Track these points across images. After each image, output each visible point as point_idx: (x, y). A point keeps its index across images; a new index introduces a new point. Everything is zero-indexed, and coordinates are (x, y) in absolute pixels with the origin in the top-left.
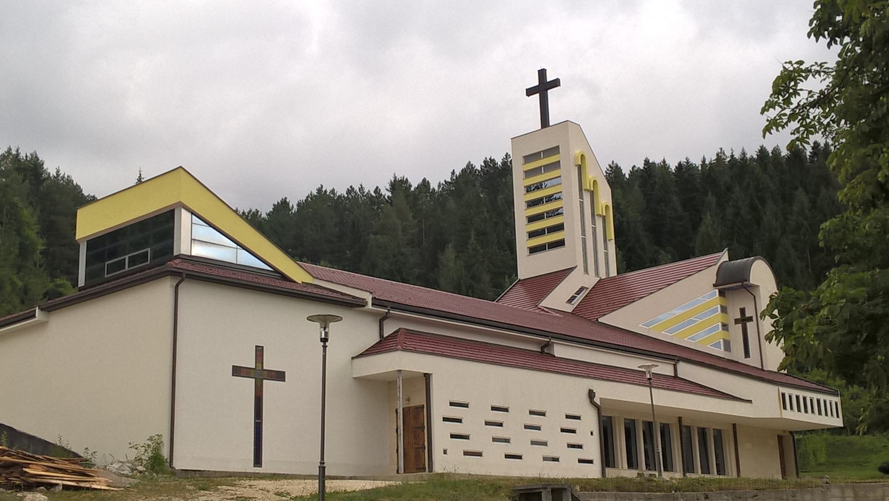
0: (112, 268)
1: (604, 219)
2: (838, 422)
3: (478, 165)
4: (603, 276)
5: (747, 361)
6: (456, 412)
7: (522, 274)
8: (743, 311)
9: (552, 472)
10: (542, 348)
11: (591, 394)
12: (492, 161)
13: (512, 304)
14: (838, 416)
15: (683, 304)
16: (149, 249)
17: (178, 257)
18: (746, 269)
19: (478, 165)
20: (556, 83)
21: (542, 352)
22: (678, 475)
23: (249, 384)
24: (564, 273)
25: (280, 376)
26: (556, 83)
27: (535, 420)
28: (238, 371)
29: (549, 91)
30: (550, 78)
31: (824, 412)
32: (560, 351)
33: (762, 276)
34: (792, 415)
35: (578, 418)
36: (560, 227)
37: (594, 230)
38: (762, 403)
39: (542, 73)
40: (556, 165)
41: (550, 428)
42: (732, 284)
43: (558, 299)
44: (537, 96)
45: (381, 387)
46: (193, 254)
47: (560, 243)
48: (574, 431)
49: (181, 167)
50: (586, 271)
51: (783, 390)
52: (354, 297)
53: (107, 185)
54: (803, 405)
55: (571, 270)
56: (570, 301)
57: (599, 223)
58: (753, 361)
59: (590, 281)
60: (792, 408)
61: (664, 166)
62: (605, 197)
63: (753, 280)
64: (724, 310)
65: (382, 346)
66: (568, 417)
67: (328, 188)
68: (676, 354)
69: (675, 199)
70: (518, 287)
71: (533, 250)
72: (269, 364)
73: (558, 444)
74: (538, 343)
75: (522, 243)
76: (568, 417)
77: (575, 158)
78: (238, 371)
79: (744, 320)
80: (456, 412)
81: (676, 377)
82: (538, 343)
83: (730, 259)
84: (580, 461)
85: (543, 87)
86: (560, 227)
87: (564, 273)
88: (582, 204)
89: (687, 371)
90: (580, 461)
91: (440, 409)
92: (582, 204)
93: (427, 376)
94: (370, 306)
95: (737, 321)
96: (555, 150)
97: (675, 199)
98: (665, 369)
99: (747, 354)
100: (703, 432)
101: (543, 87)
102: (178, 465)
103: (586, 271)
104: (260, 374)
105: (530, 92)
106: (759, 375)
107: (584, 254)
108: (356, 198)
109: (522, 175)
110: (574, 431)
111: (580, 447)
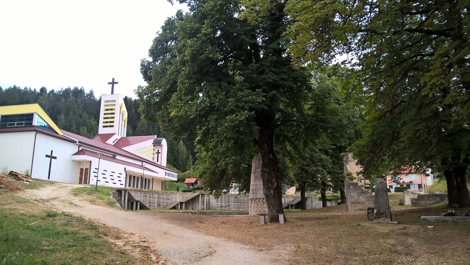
0: (9, 125)
2: (176, 180)
3: (72, 88)
7: (100, 133)
8: (158, 151)
9: (107, 185)
11: (125, 169)
13: (95, 142)
15: (144, 147)
17: (34, 126)
18: (161, 141)
19: (72, 88)
20: (117, 83)
24: (113, 134)
26: (117, 83)
27: (112, 174)
28: (47, 156)
31: (173, 176)
32: (118, 157)
33: (164, 142)
34: (167, 177)
36: (113, 122)
38: (161, 174)
39: (113, 79)
41: (116, 175)
42: (157, 144)
43: (111, 141)
47: (113, 126)
54: (169, 175)
55: (114, 134)
57: (123, 122)
58: (159, 163)
59: (119, 137)
61: (131, 99)
64: (154, 150)
65: (78, 153)
67: (17, 86)
69: (133, 110)
70: (98, 136)
71: (104, 127)
73: (116, 180)
75: (101, 124)
78: (47, 156)
79: (158, 153)
85: (113, 83)
86: (113, 122)
87: (113, 134)
91: (93, 169)
93: (91, 162)
94: (77, 143)
97: (133, 110)
98: (140, 163)
99: (158, 161)
100: (134, 177)
101: (113, 83)
102: (32, 177)
104: (51, 157)
105: (109, 83)
106: (160, 167)
107: (119, 129)
108: (27, 91)
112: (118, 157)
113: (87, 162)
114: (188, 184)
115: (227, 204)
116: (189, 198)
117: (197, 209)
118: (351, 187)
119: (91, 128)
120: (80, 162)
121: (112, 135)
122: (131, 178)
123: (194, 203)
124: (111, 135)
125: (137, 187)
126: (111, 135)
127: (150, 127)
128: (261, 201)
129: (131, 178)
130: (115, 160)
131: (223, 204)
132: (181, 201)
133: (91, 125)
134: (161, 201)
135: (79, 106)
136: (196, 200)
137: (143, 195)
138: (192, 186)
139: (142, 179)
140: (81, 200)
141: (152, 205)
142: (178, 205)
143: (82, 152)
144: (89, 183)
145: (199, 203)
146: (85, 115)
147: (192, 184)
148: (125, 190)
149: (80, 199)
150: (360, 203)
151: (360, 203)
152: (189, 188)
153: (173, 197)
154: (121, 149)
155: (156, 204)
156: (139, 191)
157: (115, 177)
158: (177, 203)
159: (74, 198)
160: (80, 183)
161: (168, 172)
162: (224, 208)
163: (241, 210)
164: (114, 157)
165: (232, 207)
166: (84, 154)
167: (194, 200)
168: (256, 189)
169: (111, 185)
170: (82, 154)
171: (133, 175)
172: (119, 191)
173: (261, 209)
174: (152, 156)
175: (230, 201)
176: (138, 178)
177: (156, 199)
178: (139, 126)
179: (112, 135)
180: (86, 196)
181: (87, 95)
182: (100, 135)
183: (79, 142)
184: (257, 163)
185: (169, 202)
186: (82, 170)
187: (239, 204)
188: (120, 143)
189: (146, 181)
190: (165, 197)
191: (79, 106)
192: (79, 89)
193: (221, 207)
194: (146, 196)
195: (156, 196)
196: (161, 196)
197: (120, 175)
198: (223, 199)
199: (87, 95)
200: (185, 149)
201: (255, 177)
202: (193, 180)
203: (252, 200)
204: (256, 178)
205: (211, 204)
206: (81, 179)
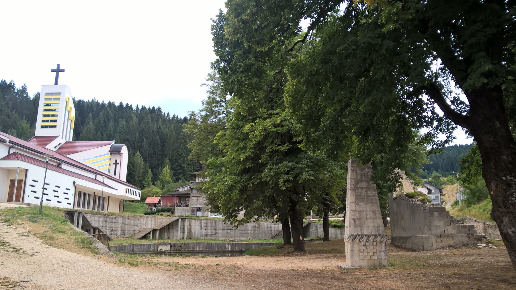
4: (68, 141)
6: (34, 183)
7: (37, 134)
8: (116, 161)
11: (74, 182)
12: (5, 81)
13: (32, 144)
15: (97, 155)
20: (63, 71)
21: (58, 166)
24: (55, 137)
26: (63, 71)
27: (57, 189)
30: (61, 68)
31: (135, 194)
32: (64, 166)
33: (124, 150)
34: (128, 195)
35: (37, 182)
37: (68, 124)
39: (58, 66)
40: (58, 99)
41: (61, 191)
42: (115, 151)
43: (52, 146)
44: (55, 73)
47: (55, 126)
48: (34, 186)
50: (62, 138)
51: (127, 187)
54: (131, 193)
55: (57, 136)
56: (55, 147)
57: (70, 122)
58: (117, 177)
59: (63, 142)
63: (122, 152)
64: (110, 159)
65: (8, 157)
66: (33, 181)
68: (96, 173)
70: (35, 139)
71: (42, 127)
74: (57, 163)
76: (33, 181)
77: (66, 99)
79: (116, 163)
80: (34, 183)
81: (96, 179)
82: (57, 163)
83: (116, 143)
84: (35, 198)
85: (58, 71)
87: (55, 137)
88: (65, 114)
89: (99, 178)
90: (35, 198)
91: (29, 182)
92: (65, 114)
93: (27, 170)
94: (8, 143)
95: (113, 164)
96: (59, 94)
98: (93, 176)
99: (115, 174)
100: (85, 194)
101: (58, 71)
103: (62, 138)
105: (53, 71)
107: (63, 131)
109: (44, 99)
110: (34, 186)
111: (36, 192)
112: (64, 166)
113: (21, 170)
114: (149, 204)
115: (214, 231)
116: (165, 224)
117: (175, 238)
118: (436, 214)
119: (22, 132)
120: (9, 171)
121: (53, 138)
122: (81, 195)
123: (171, 230)
124: (51, 138)
125: (88, 208)
126: (51, 138)
127: (99, 134)
128: (371, 239)
129: (81, 195)
130: (61, 170)
131: (209, 231)
132: (153, 227)
133: (22, 128)
134: (127, 227)
135: (7, 104)
136: (173, 226)
137: (102, 219)
138: (155, 207)
139: (95, 197)
140: (22, 234)
141: (114, 234)
142: (150, 233)
143: (15, 157)
144: (23, 201)
145: (177, 231)
146: (15, 115)
147: (155, 205)
148: (79, 213)
149: (20, 231)
150: (448, 236)
151: (448, 236)
152: (151, 209)
153: (142, 223)
154: (66, 157)
155: (119, 233)
156: (98, 214)
157: (60, 193)
158: (149, 231)
159: (6, 229)
160: (10, 200)
162: (209, 237)
163: (232, 239)
164: (59, 166)
165: (220, 235)
166: (17, 159)
167: (171, 227)
168: (360, 219)
169: (54, 203)
170: (14, 159)
171: (83, 191)
173: (371, 254)
174: (108, 167)
175: (217, 228)
176: (89, 195)
177: (120, 225)
178: (85, 131)
179: (53, 138)
180: (29, 226)
181: (18, 90)
182: (37, 137)
183: (11, 142)
184: (359, 171)
185: (137, 229)
186: (12, 182)
187: (229, 231)
188: (64, 149)
189: (100, 200)
190: (132, 221)
191: (7, 104)
192: (8, 82)
193: (206, 235)
194: (106, 221)
195: (120, 221)
196: (127, 221)
197: (67, 191)
198: (209, 224)
199: (18, 90)
200: (143, 162)
201: (357, 196)
202: (156, 200)
203: (355, 238)
204: (358, 198)
205: (193, 231)
206: (10, 195)
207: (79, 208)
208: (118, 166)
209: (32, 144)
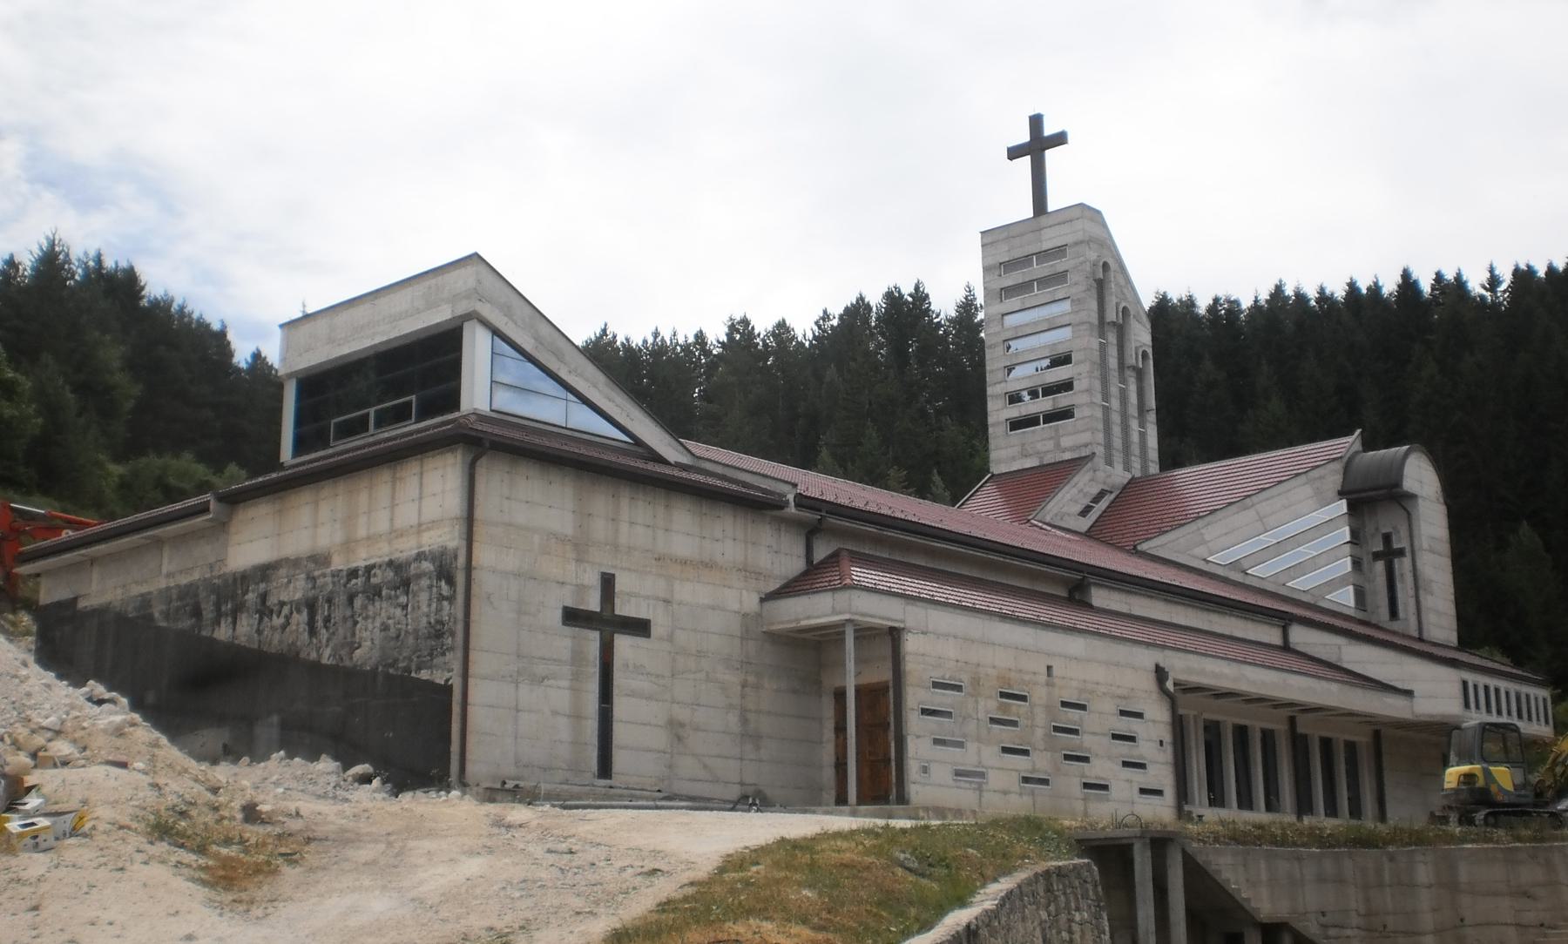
1: (1140, 374)
4: (1138, 474)
5: (1395, 626)
7: (996, 469)
8: (1387, 538)
10: (1070, 592)
13: (980, 515)
14: (1547, 722)
15: (1281, 521)
16: (413, 398)
20: (1060, 139)
22: (1289, 818)
23: (592, 639)
25: (640, 627)
26: (1060, 139)
29: (1048, 152)
30: (1049, 130)
32: (1100, 597)
33: (1420, 476)
39: (1036, 122)
42: (1371, 499)
44: (1026, 161)
45: (811, 650)
46: (991, 430)
47: (1066, 414)
49: (475, 258)
52: (764, 491)
53: (269, 278)
56: (1085, 512)
60: (1477, 707)
62: (1142, 336)
70: (989, 488)
72: (624, 608)
81: (1286, 648)
83: (1368, 445)
85: (1037, 145)
91: (915, 697)
95: (1377, 556)
99: (1394, 614)
101: (1037, 145)
104: (604, 621)
106: (1419, 648)
107: (1109, 431)
112: (1100, 597)
113: (866, 634)
122: (1219, 744)
126: (1054, 474)
129: (1219, 744)
139: (1299, 743)
148: (1160, 843)
161: (1482, 680)
172: (1111, 855)
176: (1268, 737)
183: (803, 501)
188: (1121, 514)
207: (1248, 816)
208: (1403, 566)
209: (980, 515)
